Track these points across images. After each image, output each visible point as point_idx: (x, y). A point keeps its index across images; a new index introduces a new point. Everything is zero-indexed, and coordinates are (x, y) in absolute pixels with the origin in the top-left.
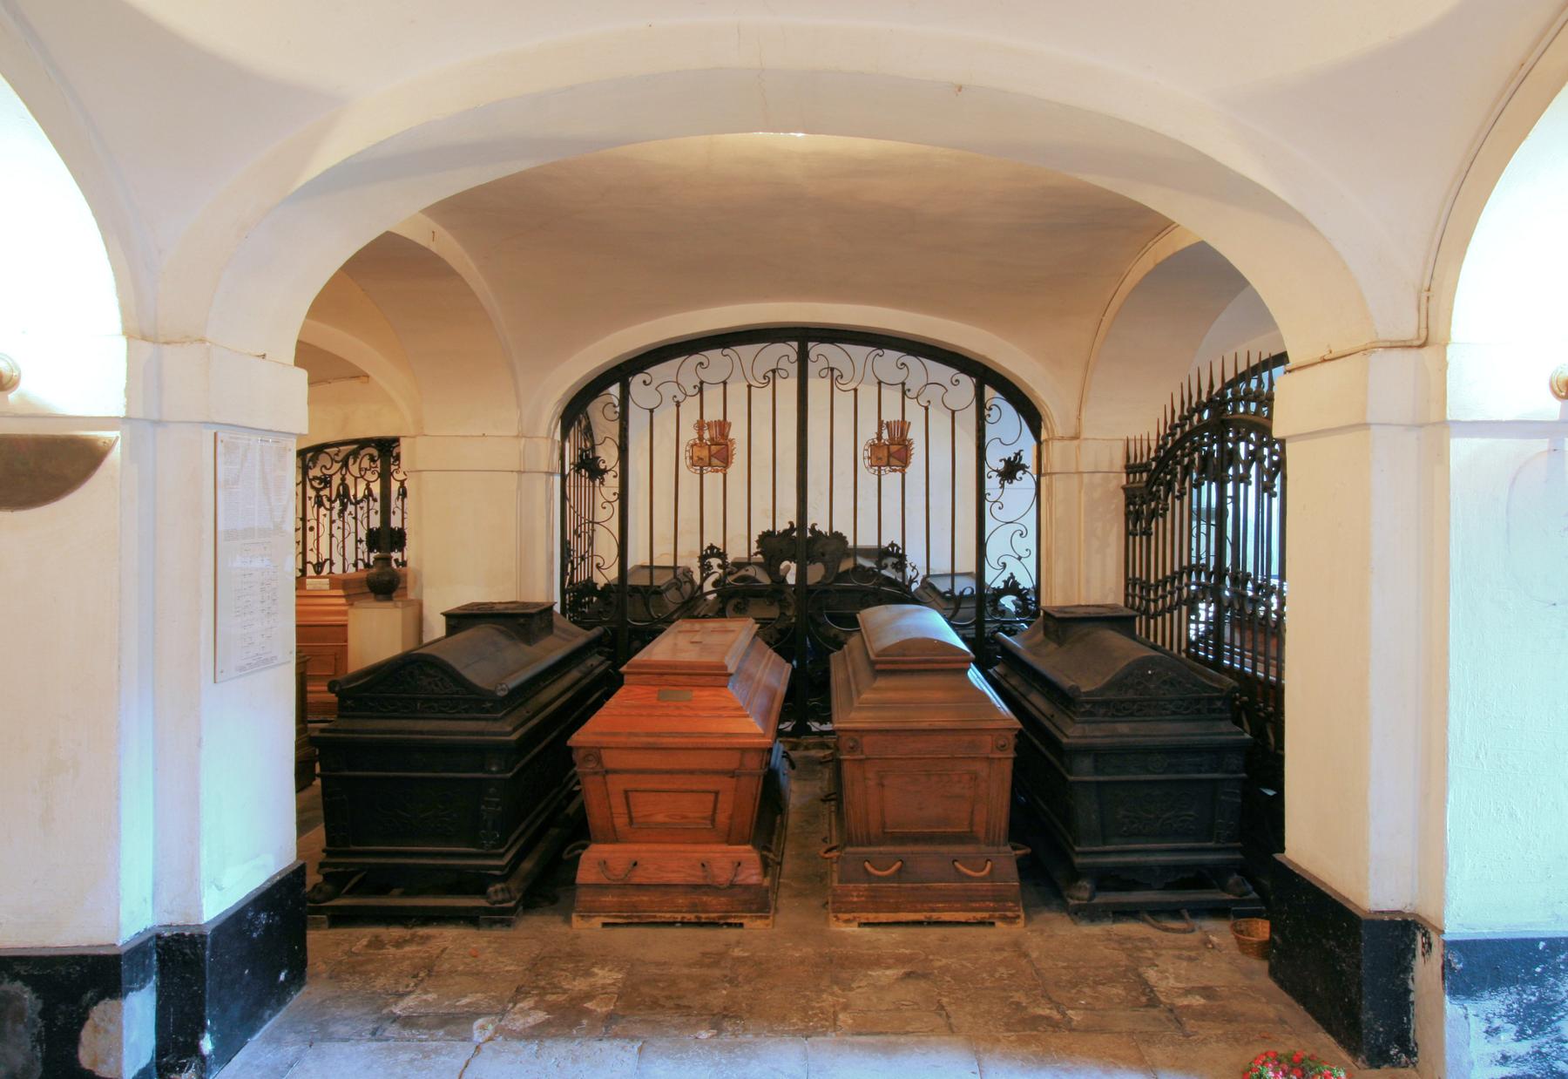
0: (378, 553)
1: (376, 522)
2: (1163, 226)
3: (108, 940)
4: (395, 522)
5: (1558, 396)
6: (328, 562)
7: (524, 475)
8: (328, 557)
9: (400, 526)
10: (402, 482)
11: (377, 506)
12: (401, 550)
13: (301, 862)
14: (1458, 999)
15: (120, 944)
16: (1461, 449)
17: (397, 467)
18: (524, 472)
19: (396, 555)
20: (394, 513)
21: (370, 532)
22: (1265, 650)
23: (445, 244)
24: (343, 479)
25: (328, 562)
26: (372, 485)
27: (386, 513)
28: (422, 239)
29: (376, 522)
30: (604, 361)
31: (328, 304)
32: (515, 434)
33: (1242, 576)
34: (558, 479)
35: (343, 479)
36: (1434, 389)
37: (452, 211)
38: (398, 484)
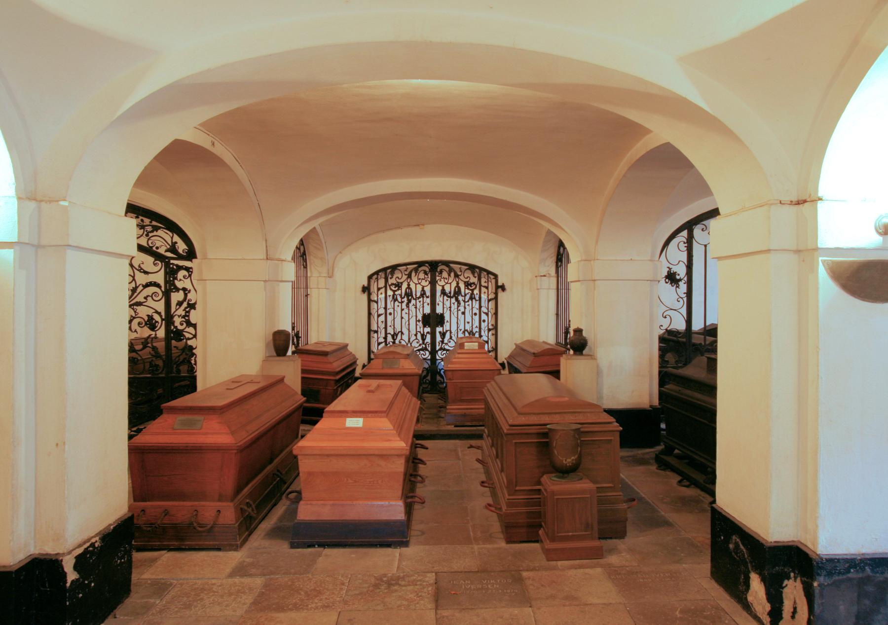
1: (427, 310)
2: (645, 131)
4: (439, 310)
5: (880, 234)
9: (442, 312)
10: (443, 286)
11: (428, 300)
12: (442, 326)
20: (438, 304)
24: (458, 283)
26: (425, 289)
27: (433, 304)
29: (427, 310)
31: (144, 180)
35: (458, 283)
37: (208, 126)
38: (441, 288)
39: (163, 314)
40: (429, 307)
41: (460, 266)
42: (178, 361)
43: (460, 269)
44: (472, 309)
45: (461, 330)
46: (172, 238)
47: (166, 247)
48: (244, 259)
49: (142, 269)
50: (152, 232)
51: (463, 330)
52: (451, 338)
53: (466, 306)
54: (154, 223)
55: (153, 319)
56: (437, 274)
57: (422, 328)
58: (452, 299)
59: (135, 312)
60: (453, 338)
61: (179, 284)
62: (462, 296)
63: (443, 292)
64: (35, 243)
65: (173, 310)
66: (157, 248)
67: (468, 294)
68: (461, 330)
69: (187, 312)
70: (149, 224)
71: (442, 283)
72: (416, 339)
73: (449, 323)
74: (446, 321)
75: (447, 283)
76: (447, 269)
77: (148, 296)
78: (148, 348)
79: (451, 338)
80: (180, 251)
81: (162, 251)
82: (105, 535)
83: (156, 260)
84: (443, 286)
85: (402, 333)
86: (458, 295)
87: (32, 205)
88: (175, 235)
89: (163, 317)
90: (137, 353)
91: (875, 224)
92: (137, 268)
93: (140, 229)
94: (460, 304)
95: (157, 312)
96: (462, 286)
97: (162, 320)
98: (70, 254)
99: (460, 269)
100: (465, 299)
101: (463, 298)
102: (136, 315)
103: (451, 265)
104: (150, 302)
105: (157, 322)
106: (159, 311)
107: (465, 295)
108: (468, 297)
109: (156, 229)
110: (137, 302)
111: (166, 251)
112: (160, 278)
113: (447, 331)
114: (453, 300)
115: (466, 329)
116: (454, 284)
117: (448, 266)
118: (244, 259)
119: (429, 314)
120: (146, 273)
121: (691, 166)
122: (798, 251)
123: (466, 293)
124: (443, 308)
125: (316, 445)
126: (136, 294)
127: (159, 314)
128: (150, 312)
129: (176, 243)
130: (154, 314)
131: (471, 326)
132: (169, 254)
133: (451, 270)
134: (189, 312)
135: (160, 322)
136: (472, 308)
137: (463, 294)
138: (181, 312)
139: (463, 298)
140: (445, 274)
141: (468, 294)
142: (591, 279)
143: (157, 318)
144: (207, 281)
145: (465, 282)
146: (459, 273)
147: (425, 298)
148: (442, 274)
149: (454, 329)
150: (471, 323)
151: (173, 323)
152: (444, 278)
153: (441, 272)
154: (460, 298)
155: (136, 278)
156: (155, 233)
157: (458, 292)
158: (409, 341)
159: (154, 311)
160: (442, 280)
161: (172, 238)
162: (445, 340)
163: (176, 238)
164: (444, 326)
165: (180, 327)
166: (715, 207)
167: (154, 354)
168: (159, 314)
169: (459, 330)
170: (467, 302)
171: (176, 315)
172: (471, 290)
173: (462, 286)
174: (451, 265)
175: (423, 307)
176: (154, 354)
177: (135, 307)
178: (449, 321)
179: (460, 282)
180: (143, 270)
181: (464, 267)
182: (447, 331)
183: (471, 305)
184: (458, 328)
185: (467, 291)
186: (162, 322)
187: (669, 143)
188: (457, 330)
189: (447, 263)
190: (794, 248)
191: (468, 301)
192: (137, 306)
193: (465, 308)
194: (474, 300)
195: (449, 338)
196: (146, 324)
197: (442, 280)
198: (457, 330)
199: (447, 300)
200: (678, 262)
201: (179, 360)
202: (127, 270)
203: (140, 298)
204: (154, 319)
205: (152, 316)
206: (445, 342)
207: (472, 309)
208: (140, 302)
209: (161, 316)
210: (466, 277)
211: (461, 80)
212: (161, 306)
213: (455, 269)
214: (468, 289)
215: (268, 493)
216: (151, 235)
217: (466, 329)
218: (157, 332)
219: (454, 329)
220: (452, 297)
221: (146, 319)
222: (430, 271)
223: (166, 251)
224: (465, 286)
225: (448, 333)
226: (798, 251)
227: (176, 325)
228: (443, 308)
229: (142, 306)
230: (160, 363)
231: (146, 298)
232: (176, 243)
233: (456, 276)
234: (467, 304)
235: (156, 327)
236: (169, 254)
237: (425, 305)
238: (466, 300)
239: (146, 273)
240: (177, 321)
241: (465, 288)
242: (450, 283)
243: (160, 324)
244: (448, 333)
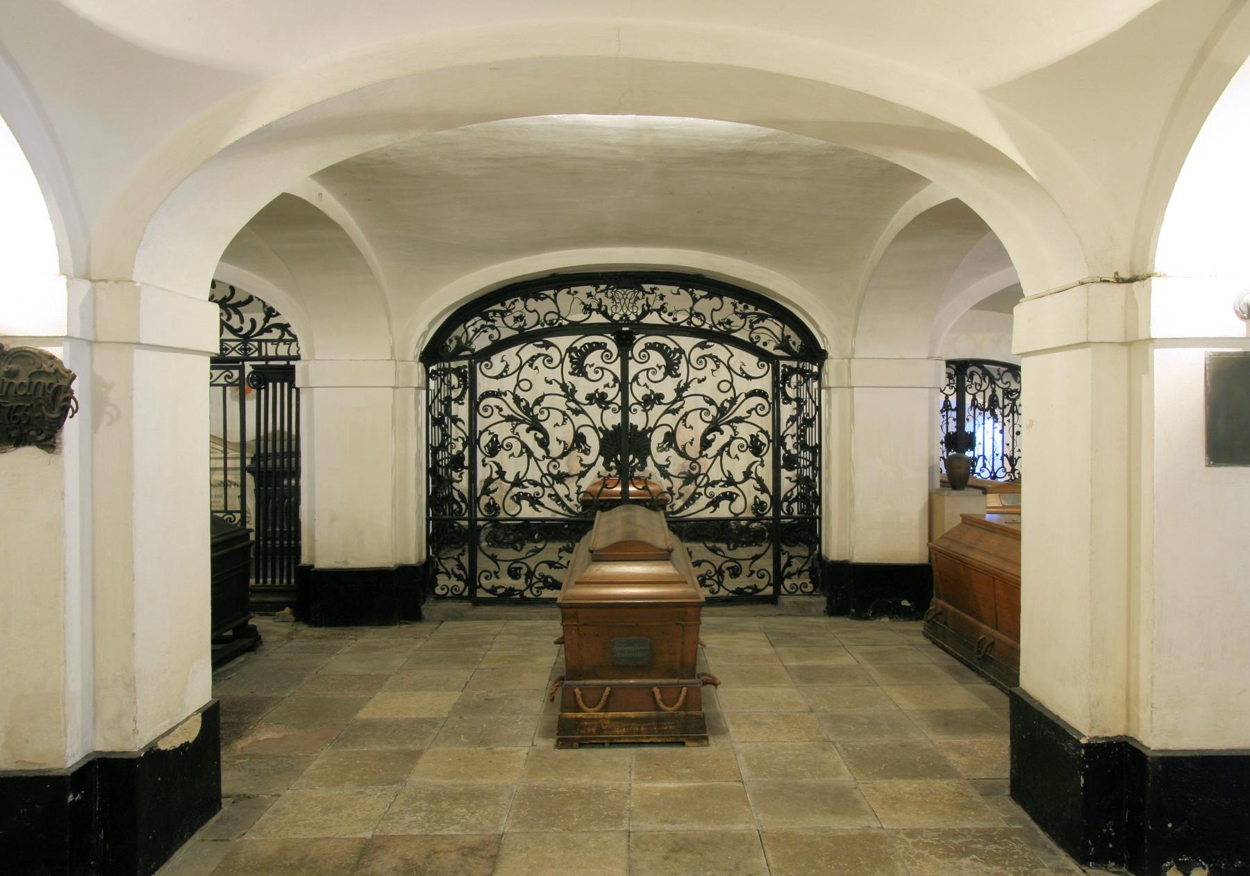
0: (955, 453)
1: (952, 428)
2: (915, 181)
3: (59, 765)
4: (969, 428)
5: (1243, 318)
6: (982, 457)
7: (398, 390)
8: (981, 453)
9: (972, 431)
10: (974, 395)
11: (954, 414)
12: (973, 449)
13: (216, 700)
14: (439, 786)
15: (69, 764)
16: (1159, 355)
17: (970, 383)
18: (398, 388)
19: (969, 454)
20: (968, 420)
21: (948, 436)
22: (746, 520)
23: (330, 204)
24: (994, 391)
25: (982, 457)
26: (950, 398)
27: (961, 420)
28: (313, 200)
29: (952, 428)
30: (464, 296)
31: (236, 251)
32: (926, 356)
33: (968, 459)
34: (424, 392)
35: (994, 391)
36: (1135, 314)
37: (333, 175)
38: (971, 397)
39: (770, 433)
40: (955, 424)
41: (998, 367)
42: (790, 497)
43: (998, 370)
44: (1013, 426)
45: (997, 455)
46: (783, 329)
47: (776, 342)
48: (904, 359)
49: (744, 372)
50: (757, 322)
51: (1000, 455)
52: (984, 466)
53: (1005, 421)
54: (760, 311)
55: (757, 440)
56: (966, 379)
57: (945, 453)
58: (986, 413)
59: (734, 430)
60: (987, 467)
61: (791, 393)
62: (1000, 408)
63: (974, 405)
64: (91, 338)
65: (783, 428)
66: (765, 344)
67: (1008, 405)
68: (997, 455)
69: (802, 431)
70: (753, 311)
71: (973, 390)
72: (1003, 466)
73: (982, 446)
74: (977, 443)
75: (979, 391)
76: (980, 371)
77: (752, 409)
78: (751, 480)
79: (984, 466)
80: (795, 348)
81: (770, 348)
82: (220, 742)
83: (760, 360)
84: (974, 395)
85: (984, 458)
86: (995, 408)
87: (85, 286)
88: (786, 326)
89: (771, 438)
90: (736, 487)
91: (1235, 307)
92: (739, 372)
93: (741, 318)
94: (997, 419)
95: (762, 431)
96: (999, 393)
97: (769, 441)
98: (139, 354)
99: (998, 370)
100: (1003, 411)
101: (1001, 411)
102: (735, 435)
103: (985, 366)
104: (754, 418)
105: (764, 445)
106: (765, 430)
107: (1004, 407)
108: (1007, 411)
109: (762, 318)
110: (736, 417)
111: (776, 348)
112: (766, 384)
113: (979, 456)
114: (988, 414)
115: (1005, 453)
116: (989, 393)
117: (981, 367)
118: (904, 359)
119: (955, 434)
120: (749, 377)
121: (989, 229)
122: (1127, 344)
123: (1005, 404)
124: (975, 425)
125: (772, 619)
126: (735, 407)
127: (766, 433)
128: (755, 431)
129: (789, 337)
130: (760, 434)
131: (1011, 448)
132: (779, 353)
133: (986, 373)
134: (804, 431)
135: (767, 443)
136: (1013, 425)
137: (1001, 406)
138: (793, 430)
139: (1001, 411)
140: (977, 379)
141: (1008, 405)
142: (846, 385)
143: (763, 438)
144: (315, 389)
145: (1004, 389)
146: (997, 377)
147: (949, 412)
148: (972, 377)
149: (988, 454)
150: (1011, 445)
151: (784, 446)
152: (976, 384)
153: (971, 376)
154: (998, 411)
155: (734, 384)
156: (761, 324)
157: (993, 402)
158: (993, 469)
159: (759, 430)
160: (973, 386)
161: (783, 329)
162: (976, 468)
163: (788, 331)
164: (976, 449)
165: (794, 452)
166: (1017, 282)
167: (759, 487)
168: (766, 433)
169: (995, 455)
170: (1006, 416)
171: (788, 435)
172: (1011, 400)
173: (999, 393)
174: (985, 366)
175: (947, 423)
176: (759, 487)
177: (735, 424)
178: (982, 442)
179: (997, 388)
180: (746, 373)
181: (1003, 369)
182: (979, 456)
183: (1011, 421)
184: (994, 452)
185: (1007, 402)
186: (769, 444)
187: (957, 199)
188: (993, 455)
189: (979, 363)
190: (1119, 338)
191: (1008, 415)
192: (737, 422)
193: (1004, 424)
194: (1016, 414)
195: (982, 465)
196: (748, 447)
197: (973, 386)
198: (993, 455)
199: (980, 414)
200: (517, 357)
201: (792, 494)
202: (824, 377)
203: (741, 412)
204: (760, 441)
205: (758, 436)
206: (976, 472)
207: (1013, 426)
208: (741, 417)
209: (768, 436)
210: (1005, 382)
211: (626, 111)
212: (766, 423)
213: (991, 371)
214: (1008, 398)
215: (632, 684)
216: (755, 326)
217: (1005, 453)
218: (764, 457)
219: (988, 454)
220: (987, 410)
221: (749, 440)
222: (955, 375)
223: (776, 348)
224: (1004, 394)
225: (981, 459)
226: (1127, 344)
227: (788, 448)
228: (975, 425)
229: (743, 423)
230: (765, 498)
231: (749, 412)
232: (789, 337)
233: (992, 381)
234: (1006, 419)
235: (761, 451)
236: (779, 353)
237: (950, 420)
238: (1005, 414)
239: (749, 377)
240: (790, 443)
241: (1003, 398)
242: (984, 391)
243: (766, 447)
244: (981, 459)
